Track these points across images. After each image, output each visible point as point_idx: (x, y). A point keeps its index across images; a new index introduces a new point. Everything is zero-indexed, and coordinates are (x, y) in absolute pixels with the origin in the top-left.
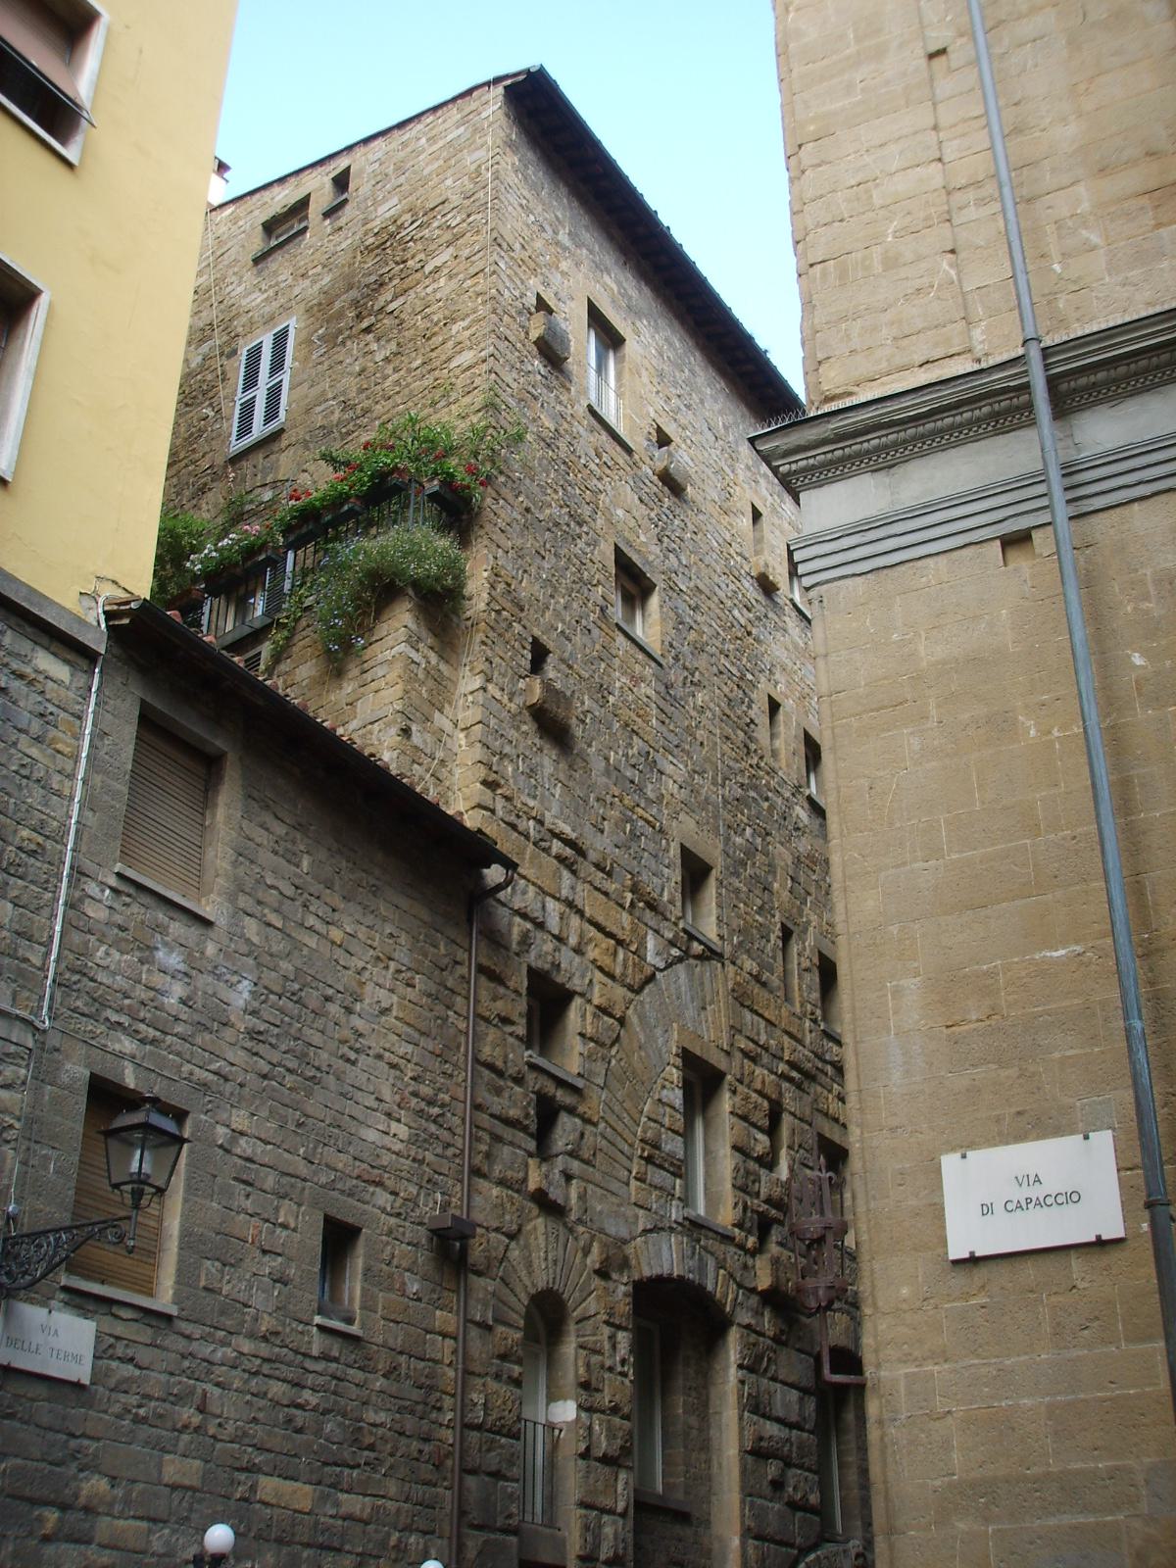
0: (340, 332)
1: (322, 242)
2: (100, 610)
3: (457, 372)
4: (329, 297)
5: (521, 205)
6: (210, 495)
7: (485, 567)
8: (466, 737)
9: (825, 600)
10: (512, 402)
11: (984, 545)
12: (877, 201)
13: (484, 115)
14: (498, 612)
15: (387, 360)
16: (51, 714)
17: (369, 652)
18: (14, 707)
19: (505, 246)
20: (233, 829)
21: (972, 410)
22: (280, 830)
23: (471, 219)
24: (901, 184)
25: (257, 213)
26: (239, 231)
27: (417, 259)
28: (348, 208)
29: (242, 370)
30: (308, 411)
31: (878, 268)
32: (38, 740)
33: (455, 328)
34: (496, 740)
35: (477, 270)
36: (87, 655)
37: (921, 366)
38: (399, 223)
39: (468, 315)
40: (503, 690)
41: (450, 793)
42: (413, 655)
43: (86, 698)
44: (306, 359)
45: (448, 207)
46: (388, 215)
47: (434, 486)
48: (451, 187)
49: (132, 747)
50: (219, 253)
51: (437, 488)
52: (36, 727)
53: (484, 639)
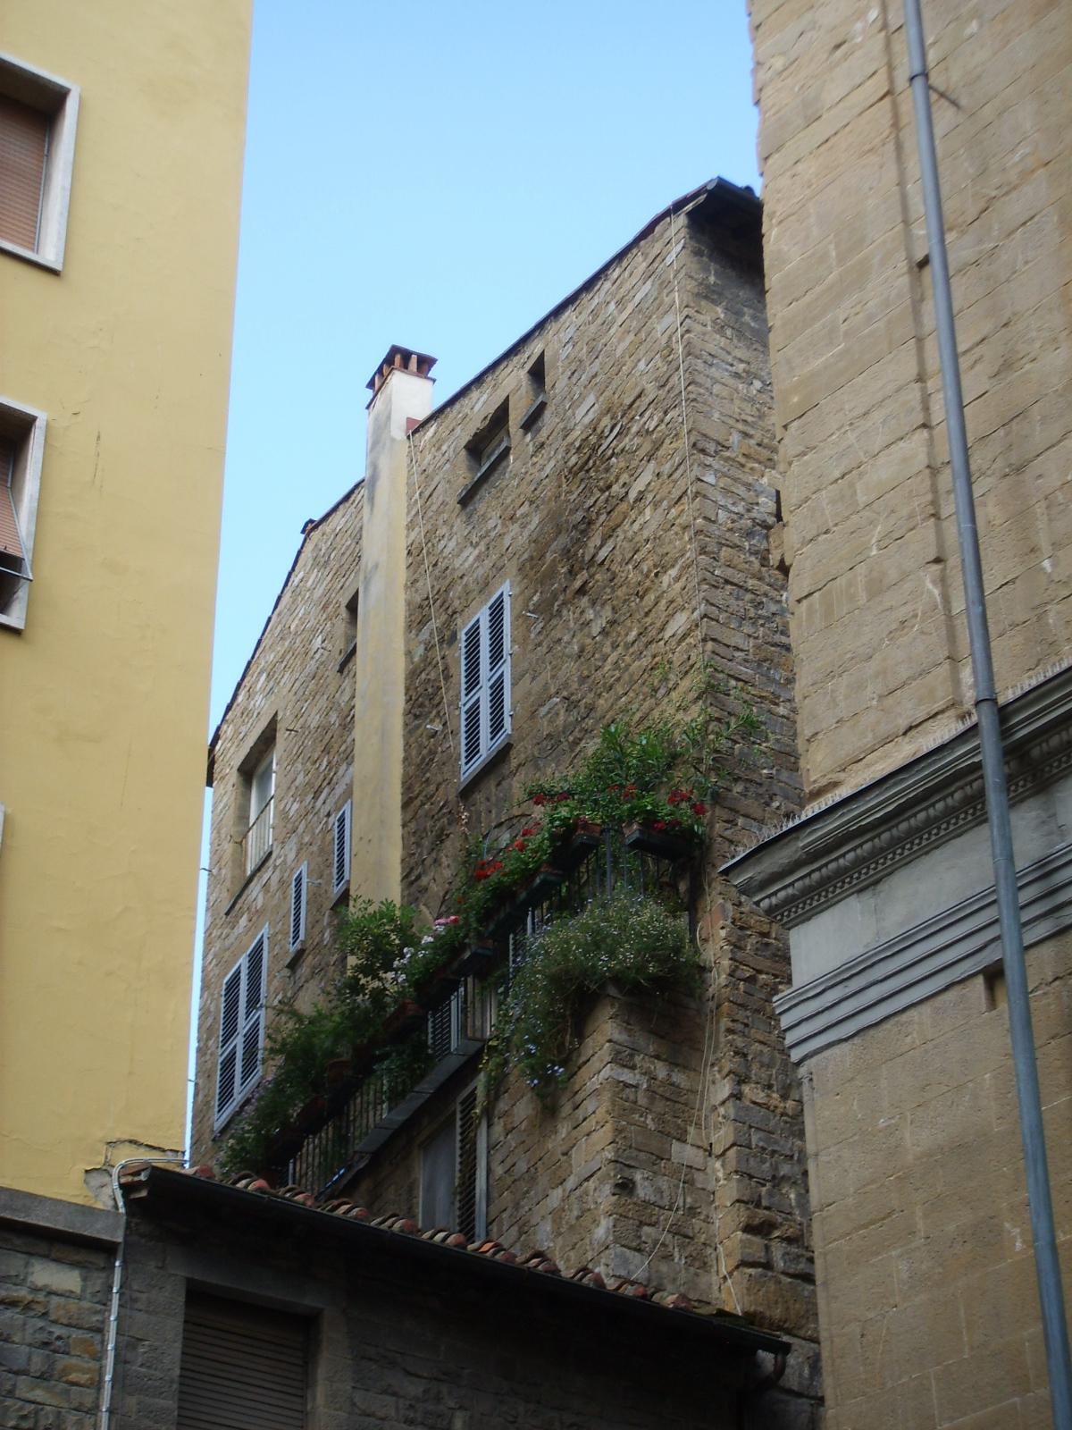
0: (555, 598)
1: (530, 465)
2: (116, 1184)
3: (673, 642)
4: (540, 545)
5: (737, 375)
6: (448, 843)
7: (721, 923)
8: (723, 1166)
9: (814, 1077)
10: (746, 671)
11: (968, 983)
12: (862, 499)
13: (668, 261)
14: (751, 980)
15: (604, 632)
16: (59, 1338)
17: (578, 1079)
18: (10, 1345)
19: (711, 447)
20: (340, 1409)
21: (944, 798)
22: (414, 1388)
23: (668, 418)
24: (883, 471)
25: (458, 430)
26: (443, 460)
27: (621, 482)
28: (547, 413)
29: (463, 662)
30: (533, 714)
31: (862, 598)
32: (43, 1377)
33: (666, 579)
34: (763, 1161)
35: (679, 493)
36: (106, 1249)
37: (905, 734)
38: (599, 431)
39: (676, 560)
40: (770, 1087)
41: (709, 1250)
42: (627, 1076)
43: (106, 1303)
44: (526, 639)
45: (646, 400)
46: (587, 420)
47: (633, 831)
48: (644, 372)
49: (178, 1345)
50: (427, 494)
51: (637, 835)
52: (38, 1362)
53: (730, 1025)
